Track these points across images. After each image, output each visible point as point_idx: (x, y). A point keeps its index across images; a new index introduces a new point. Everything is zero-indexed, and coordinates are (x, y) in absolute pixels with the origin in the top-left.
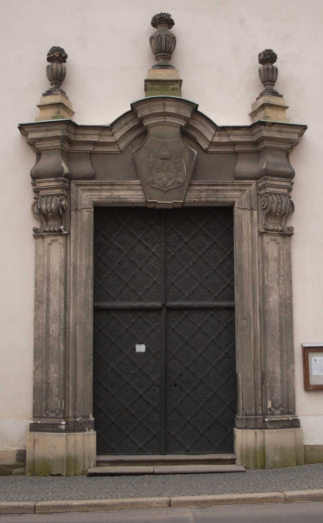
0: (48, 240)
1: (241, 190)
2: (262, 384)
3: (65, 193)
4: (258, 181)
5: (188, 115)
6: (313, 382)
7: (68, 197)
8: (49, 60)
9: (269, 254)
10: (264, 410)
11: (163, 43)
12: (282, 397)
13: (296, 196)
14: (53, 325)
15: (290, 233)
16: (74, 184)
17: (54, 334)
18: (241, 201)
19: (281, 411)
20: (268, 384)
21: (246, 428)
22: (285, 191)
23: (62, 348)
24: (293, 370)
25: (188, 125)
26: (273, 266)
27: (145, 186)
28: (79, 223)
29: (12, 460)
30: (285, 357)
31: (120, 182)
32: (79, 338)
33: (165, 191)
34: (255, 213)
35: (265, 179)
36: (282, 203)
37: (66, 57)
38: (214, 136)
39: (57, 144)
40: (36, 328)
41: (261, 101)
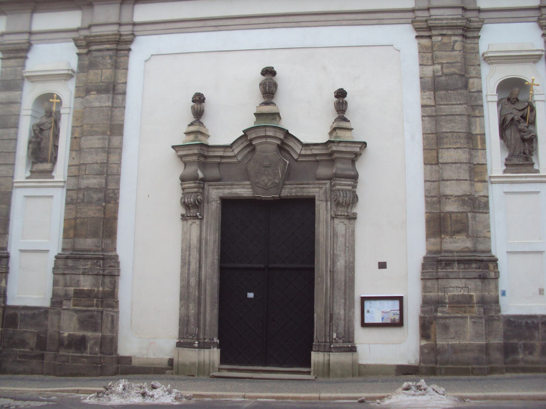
0: (190, 222)
1: (320, 188)
2: (330, 322)
3: (201, 190)
4: (183, 183)
5: (282, 137)
7: (203, 194)
8: (193, 101)
9: (338, 232)
10: (331, 340)
11: (267, 88)
12: (345, 331)
13: (359, 191)
14: (192, 278)
15: (354, 217)
16: (207, 185)
17: (192, 285)
18: (320, 195)
19: (343, 340)
20: (334, 322)
21: (318, 351)
22: (350, 188)
23: (197, 294)
24: (354, 313)
25: (283, 143)
26: (341, 240)
27: (254, 185)
28: (210, 211)
29: (165, 364)
30: (347, 304)
31: (237, 183)
32: (208, 287)
33: (266, 189)
34: (329, 203)
35: (335, 180)
36: (347, 197)
37: (204, 99)
38: (301, 150)
39: (195, 158)
40: (182, 280)
41: (335, 126)
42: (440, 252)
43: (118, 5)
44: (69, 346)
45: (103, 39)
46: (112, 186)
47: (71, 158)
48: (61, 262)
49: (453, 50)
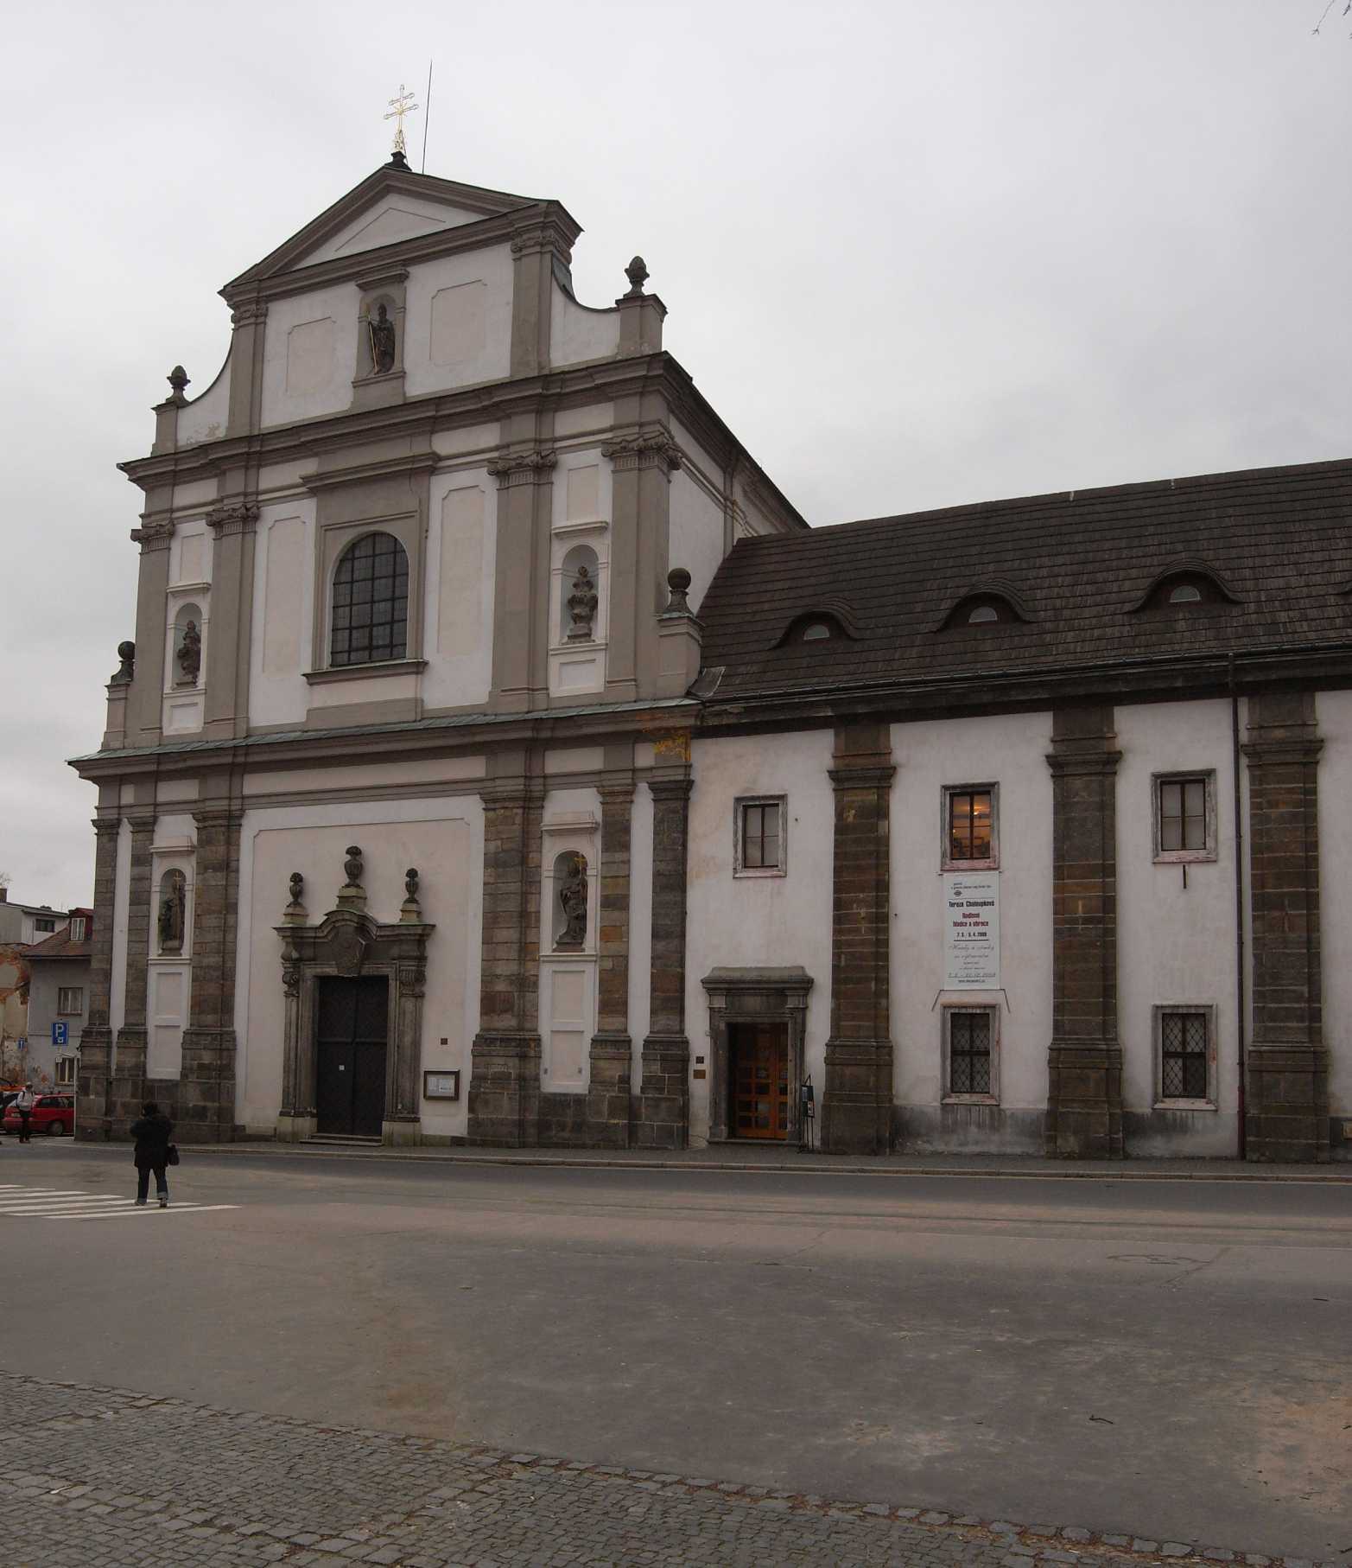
6: (429, 1094)
40: (285, 1054)
43: (227, 777)
47: (196, 936)
48: (188, 1037)
49: (514, 824)
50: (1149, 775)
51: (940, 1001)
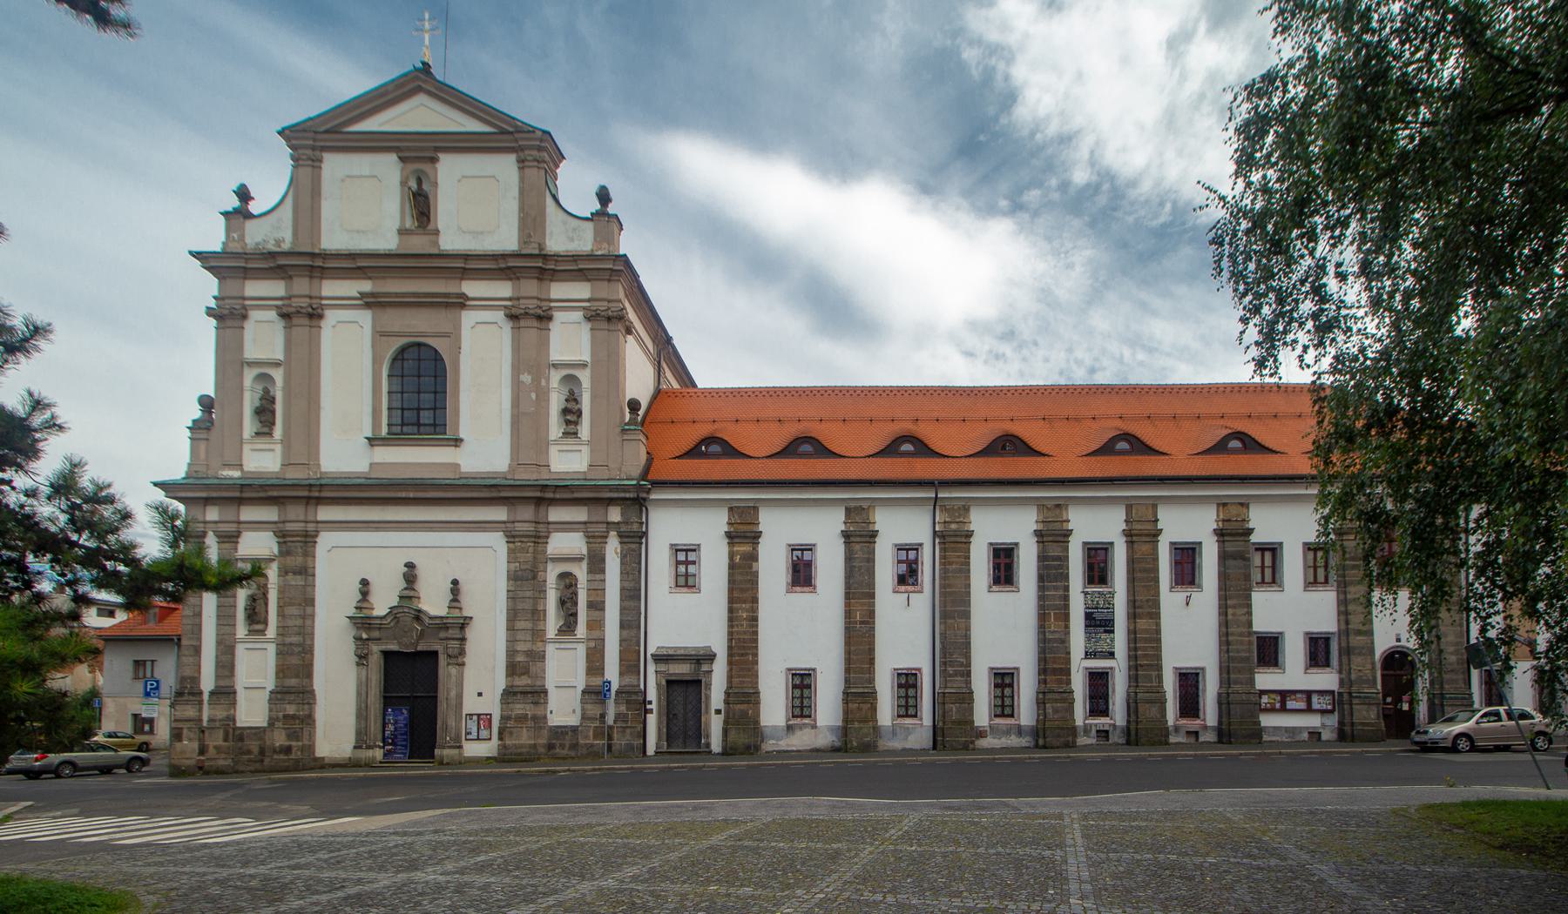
26: (454, 679)
27: (399, 643)
42: (512, 686)
44: (280, 752)
45: (295, 533)
46: (308, 642)
47: (278, 621)
50: (890, 546)
51: (1082, 665)
